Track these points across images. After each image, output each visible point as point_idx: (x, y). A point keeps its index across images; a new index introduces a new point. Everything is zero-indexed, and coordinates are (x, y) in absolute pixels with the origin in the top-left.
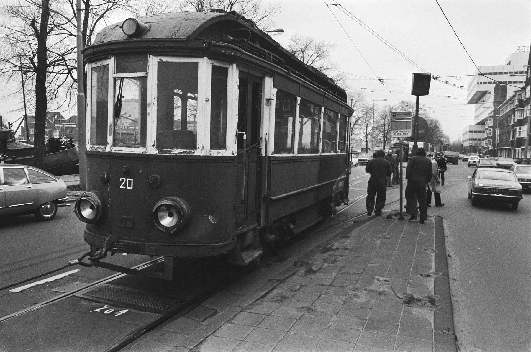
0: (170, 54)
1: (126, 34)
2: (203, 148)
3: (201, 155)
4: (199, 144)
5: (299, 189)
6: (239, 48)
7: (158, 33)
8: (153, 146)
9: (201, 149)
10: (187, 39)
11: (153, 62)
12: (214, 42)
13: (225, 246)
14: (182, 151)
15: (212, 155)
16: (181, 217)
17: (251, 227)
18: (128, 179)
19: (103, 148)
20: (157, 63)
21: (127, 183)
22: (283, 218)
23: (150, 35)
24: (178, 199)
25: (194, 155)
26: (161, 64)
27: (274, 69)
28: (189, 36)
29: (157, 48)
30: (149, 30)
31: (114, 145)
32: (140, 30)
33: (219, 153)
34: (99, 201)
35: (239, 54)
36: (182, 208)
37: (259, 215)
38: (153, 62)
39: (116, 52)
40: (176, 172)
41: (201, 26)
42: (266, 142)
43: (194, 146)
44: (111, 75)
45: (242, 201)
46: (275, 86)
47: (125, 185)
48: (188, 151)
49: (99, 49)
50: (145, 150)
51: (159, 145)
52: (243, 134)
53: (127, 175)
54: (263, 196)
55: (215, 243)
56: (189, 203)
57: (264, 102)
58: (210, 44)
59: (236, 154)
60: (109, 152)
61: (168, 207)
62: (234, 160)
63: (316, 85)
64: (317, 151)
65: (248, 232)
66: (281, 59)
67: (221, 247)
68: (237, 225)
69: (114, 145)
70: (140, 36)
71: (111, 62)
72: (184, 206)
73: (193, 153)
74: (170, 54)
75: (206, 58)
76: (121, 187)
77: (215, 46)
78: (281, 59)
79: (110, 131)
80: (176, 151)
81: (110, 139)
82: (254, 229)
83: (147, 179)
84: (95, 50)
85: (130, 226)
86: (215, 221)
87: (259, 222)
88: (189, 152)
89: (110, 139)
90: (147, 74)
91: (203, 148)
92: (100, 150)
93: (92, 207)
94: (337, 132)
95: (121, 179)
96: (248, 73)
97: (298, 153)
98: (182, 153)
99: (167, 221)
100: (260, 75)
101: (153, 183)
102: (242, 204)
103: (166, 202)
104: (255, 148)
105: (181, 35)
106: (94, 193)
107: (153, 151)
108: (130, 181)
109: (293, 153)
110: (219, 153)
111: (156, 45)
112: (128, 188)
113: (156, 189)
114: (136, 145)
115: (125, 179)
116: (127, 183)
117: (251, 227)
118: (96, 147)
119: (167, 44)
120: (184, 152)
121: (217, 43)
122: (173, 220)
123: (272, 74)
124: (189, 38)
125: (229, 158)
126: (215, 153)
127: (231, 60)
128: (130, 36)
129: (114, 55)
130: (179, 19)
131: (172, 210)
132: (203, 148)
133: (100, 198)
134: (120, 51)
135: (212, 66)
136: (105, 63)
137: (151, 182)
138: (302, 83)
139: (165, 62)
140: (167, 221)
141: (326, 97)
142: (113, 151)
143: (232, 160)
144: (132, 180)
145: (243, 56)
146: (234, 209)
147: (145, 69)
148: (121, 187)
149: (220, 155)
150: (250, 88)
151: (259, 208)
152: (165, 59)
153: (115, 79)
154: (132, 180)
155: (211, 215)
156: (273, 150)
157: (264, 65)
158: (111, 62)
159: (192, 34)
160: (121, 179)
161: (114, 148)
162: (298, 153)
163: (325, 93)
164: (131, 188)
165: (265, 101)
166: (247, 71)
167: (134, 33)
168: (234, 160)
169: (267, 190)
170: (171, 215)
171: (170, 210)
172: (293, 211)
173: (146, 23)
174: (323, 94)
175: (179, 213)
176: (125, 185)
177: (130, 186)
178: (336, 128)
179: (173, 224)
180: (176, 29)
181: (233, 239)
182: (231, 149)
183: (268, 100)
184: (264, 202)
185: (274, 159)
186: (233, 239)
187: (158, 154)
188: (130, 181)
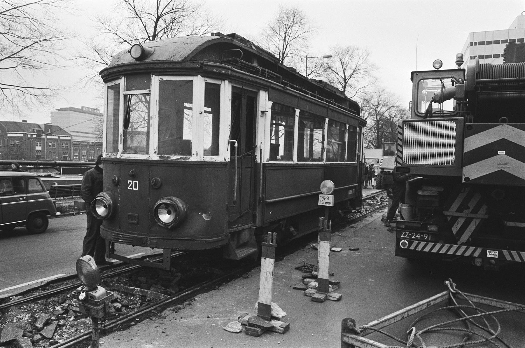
0: (169, 73)
1: (134, 58)
2: (197, 154)
3: (196, 160)
4: (194, 151)
5: (299, 194)
6: (230, 67)
7: (159, 56)
8: (155, 153)
9: (195, 155)
10: (183, 60)
11: (155, 80)
12: (206, 63)
13: (218, 241)
14: (179, 157)
15: (205, 160)
16: (177, 214)
17: (246, 227)
18: (134, 182)
19: (114, 155)
20: (158, 82)
21: (133, 185)
22: (281, 220)
23: (153, 58)
24: (175, 199)
25: (190, 160)
26: (161, 82)
27: (269, 84)
28: (185, 58)
29: (157, 69)
30: (153, 54)
31: (124, 152)
32: (145, 54)
33: (211, 158)
34: (111, 201)
35: (230, 72)
36: (178, 206)
37: (254, 216)
38: (155, 80)
39: (126, 73)
40: (177, 175)
41: (197, 49)
42: (261, 150)
43: (190, 153)
44: (122, 92)
45: (234, 201)
46: (269, 99)
47: (132, 187)
48: (184, 157)
49: (112, 71)
50: (148, 156)
51: (160, 152)
52: (235, 142)
53: (133, 177)
54: (258, 199)
55: (208, 238)
56: (186, 202)
57: (259, 114)
58: (202, 64)
59: (228, 160)
60: (119, 159)
61: (167, 206)
62: (226, 165)
63: (319, 98)
64: (322, 160)
65: (243, 230)
66: (278, 75)
67: (214, 242)
68: (231, 224)
69: (124, 152)
70: (145, 59)
71: (122, 82)
72: (180, 205)
73: (189, 158)
74: (169, 73)
75: (199, 76)
76: (129, 188)
77: (206, 65)
78: (278, 75)
79: (121, 141)
80: (174, 157)
81: (121, 147)
82: (250, 228)
83: (150, 181)
84: (110, 71)
85: (136, 222)
86: (208, 218)
87: (254, 222)
88: (185, 158)
89: (121, 147)
90: (150, 91)
91: (198, 154)
92: (113, 157)
93: (105, 206)
94: (345, 142)
95: (129, 181)
96: (242, 88)
97: (298, 161)
98: (179, 159)
99: (165, 218)
100: (256, 91)
101: (155, 185)
102: (234, 204)
103: (164, 201)
104: (249, 155)
105: (178, 57)
106: (107, 193)
107: (155, 157)
108: (136, 183)
109: (292, 160)
110: (211, 158)
111: (157, 66)
112: (134, 189)
113: (157, 189)
114: (142, 153)
115: (131, 181)
116: (133, 185)
117: (246, 227)
118: (110, 154)
119: (166, 65)
120: (181, 158)
121: (209, 63)
122: (170, 217)
123: (266, 88)
124: (185, 60)
125: (221, 163)
126: (208, 159)
127: (223, 77)
128: (137, 59)
129: (124, 75)
130: (177, 44)
131: (170, 208)
132: (197, 154)
133: (111, 198)
134: (134, 72)
135: (206, 83)
136: (117, 82)
137: (153, 184)
138: (301, 96)
139: (165, 81)
140: (165, 218)
141: (330, 109)
142: (122, 158)
143: (224, 165)
144: (137, 182)
145: (235, 74)
146: (227, 209)
147: (149, 87)
148: (129, 188)
149: (213, 160)
150: (244, 102)
151: (255, 209)
152: (165, 78)
153: (125, 96)
154: (137, 182)
155: (205, 213)
156: (268, 157)
157: (257, 80)
158: (122, 82)
159: (188, 56)
160: (129, 181)
161: (124, 155)
162: (298, 161)
163: (329, 106)
164: (137, 189)
165: (260, 113)
166: (241, 87)
167: (140, 57)
168: (226, 165)
169: (263, 193)
170: (169, 213)
171: (169, 208)
172: (293, 214)
173: (152, 48)
174: (327, 106)
175: (175, 210)
176: (132, 187)
177: (136, 187)
178: (344, 138)
179: (170, 221)
180: (176, 51)
181: (227, 236)
182: (224, 155)
183: (263, 112)
184: (259, 204)
185: (270, 165)
186: (227, 236)
187: (159, 159)
188: (136, 183)
